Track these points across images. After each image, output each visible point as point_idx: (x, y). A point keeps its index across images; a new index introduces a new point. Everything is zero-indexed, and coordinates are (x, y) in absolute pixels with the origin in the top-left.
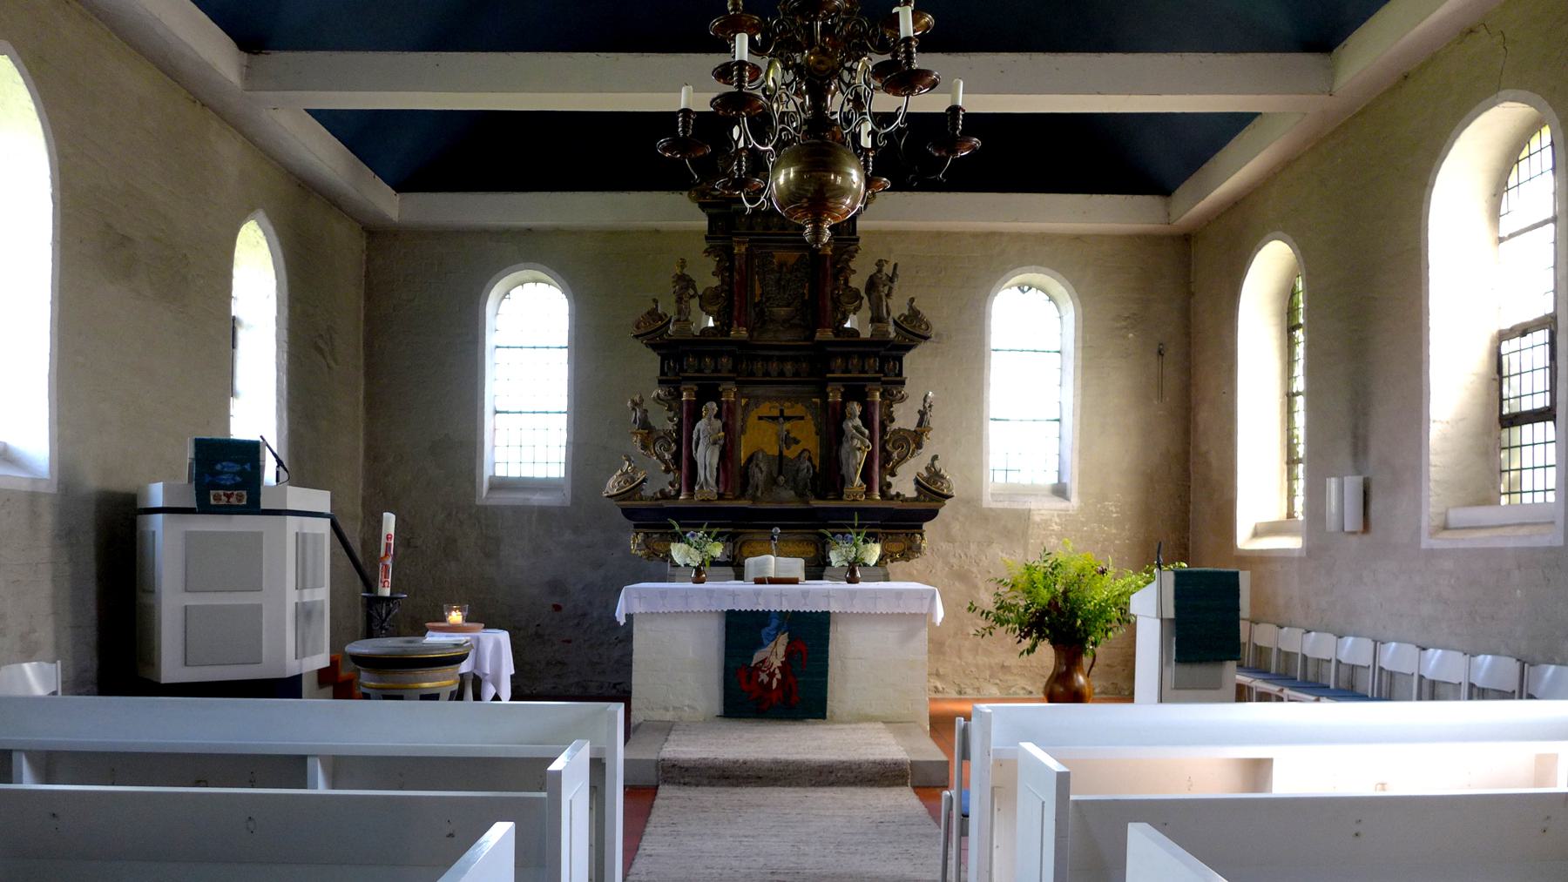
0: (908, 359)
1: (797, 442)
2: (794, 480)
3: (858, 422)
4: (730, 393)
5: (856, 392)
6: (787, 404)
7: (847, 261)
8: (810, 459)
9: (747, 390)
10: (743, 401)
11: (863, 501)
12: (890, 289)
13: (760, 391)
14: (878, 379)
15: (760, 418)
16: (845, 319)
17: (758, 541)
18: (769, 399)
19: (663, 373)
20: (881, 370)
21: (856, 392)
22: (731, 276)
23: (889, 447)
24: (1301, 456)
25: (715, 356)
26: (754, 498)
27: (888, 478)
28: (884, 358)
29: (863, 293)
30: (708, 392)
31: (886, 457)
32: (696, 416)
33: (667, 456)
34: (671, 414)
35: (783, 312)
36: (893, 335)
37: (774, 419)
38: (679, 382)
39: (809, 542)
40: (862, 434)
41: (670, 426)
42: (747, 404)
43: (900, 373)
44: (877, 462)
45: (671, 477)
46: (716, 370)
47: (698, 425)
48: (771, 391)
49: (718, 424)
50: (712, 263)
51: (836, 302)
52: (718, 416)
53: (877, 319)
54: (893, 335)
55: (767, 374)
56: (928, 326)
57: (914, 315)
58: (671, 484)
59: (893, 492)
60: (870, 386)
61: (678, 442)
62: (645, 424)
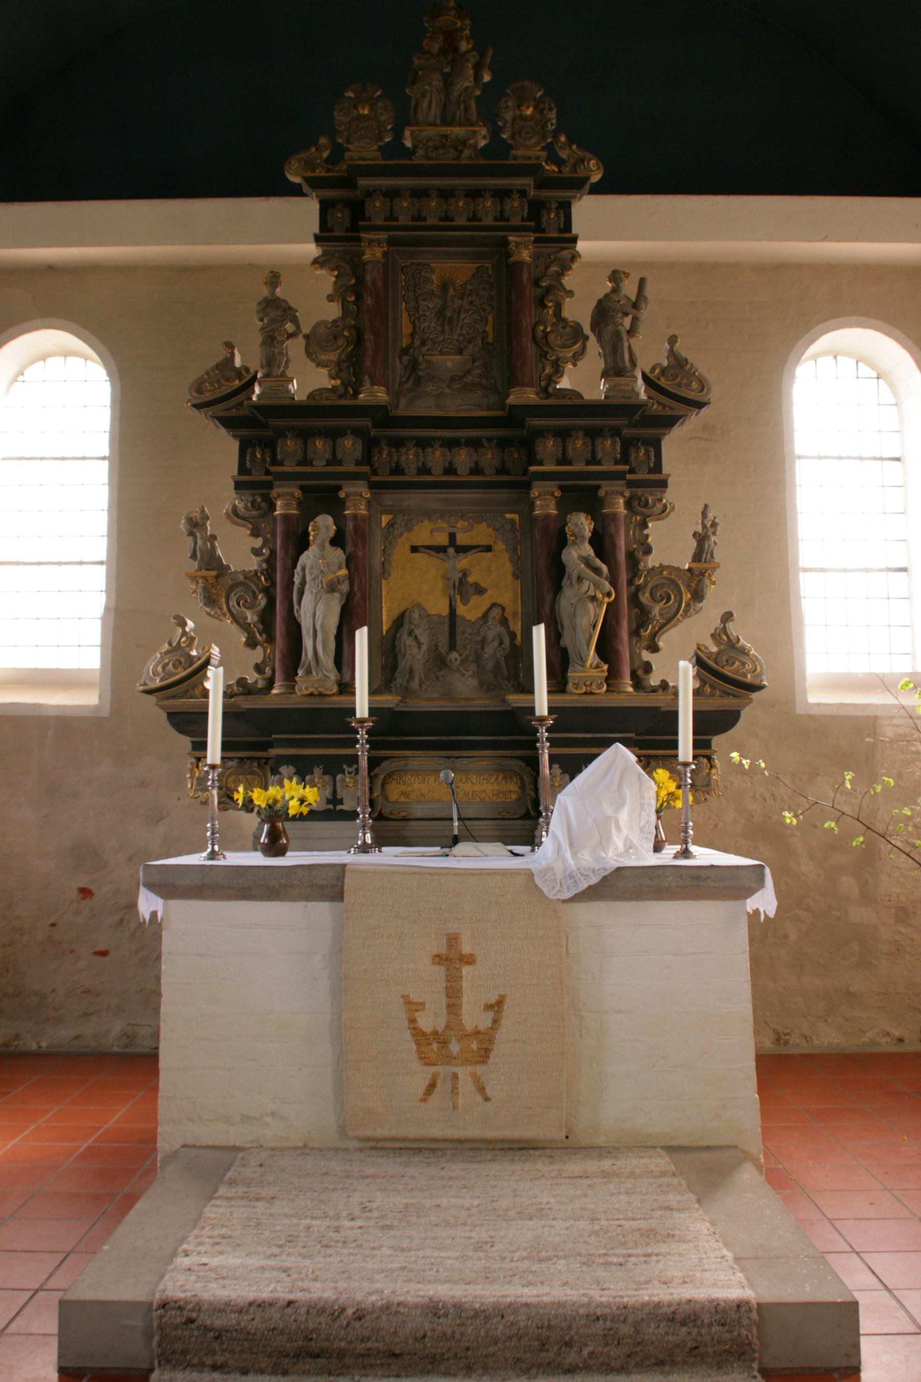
0: (672, 444)
1: (480, 590)
2: (478, 660)
3: (588, 550)
4: (357, 499)
5: (583, 496)
6: (461, 524)
7: (560, 275)
8: (504, 621)
9: (389, 498)
10: (385, 519)
11: (602, 698)
12: (635, 320)
13: (412, 499)
14: (619, 476)
15: (414, 549)
16: (558, 371)
17: (416, 773)
18: (428, 515)
19: (242, 469)
20: (625, 459)
21: (583, 496)
22: (359, 297)
23: (645, 598)
24: (664, 838)
25: (334, 435)
26: (406, 692)
27: (646, 656)
28: (636, 431)
29: (587, 330)
30: (323, 497)
31: (642, 617)
32: (300, 543)
33: (251, 617)
34: (258, 543)
35: (450, 362)
36: (643, 396)
37: (441, 549)
38: (269, 486)
39: (508, 773)
40: (597, 571)
41: (253, 564)
42: (391, 525)
43: (658, 468)
44: (625, 624)
45: (258, 655)
46: (334, 461)
47: (304, 559)
48: (432, 499)
49: (338, 555)
50: (326, 280)
51: (542, 344)
52: (338, 541)
53: (615, 370)
54: (643, 396)
55: (424, 470)
56: (703, 385)
57: (678, 364)
58: (259, 668)
59: (654, 680)
60: (606, 487)
61: (269, 593)
62: (210, 561)
